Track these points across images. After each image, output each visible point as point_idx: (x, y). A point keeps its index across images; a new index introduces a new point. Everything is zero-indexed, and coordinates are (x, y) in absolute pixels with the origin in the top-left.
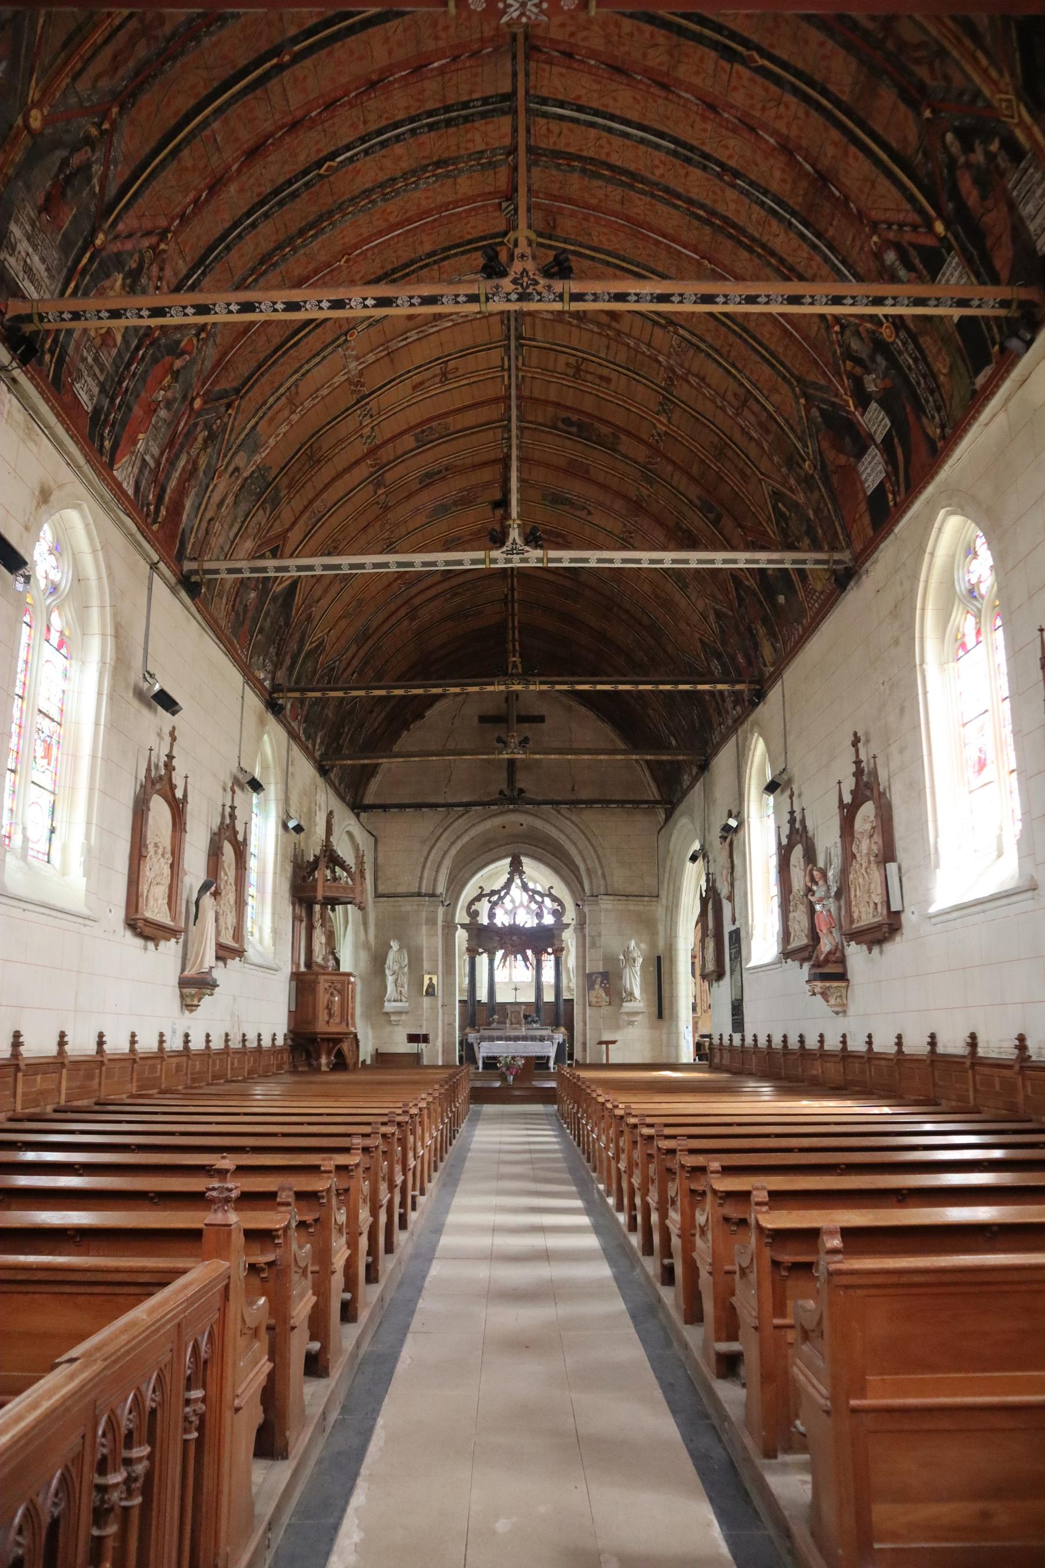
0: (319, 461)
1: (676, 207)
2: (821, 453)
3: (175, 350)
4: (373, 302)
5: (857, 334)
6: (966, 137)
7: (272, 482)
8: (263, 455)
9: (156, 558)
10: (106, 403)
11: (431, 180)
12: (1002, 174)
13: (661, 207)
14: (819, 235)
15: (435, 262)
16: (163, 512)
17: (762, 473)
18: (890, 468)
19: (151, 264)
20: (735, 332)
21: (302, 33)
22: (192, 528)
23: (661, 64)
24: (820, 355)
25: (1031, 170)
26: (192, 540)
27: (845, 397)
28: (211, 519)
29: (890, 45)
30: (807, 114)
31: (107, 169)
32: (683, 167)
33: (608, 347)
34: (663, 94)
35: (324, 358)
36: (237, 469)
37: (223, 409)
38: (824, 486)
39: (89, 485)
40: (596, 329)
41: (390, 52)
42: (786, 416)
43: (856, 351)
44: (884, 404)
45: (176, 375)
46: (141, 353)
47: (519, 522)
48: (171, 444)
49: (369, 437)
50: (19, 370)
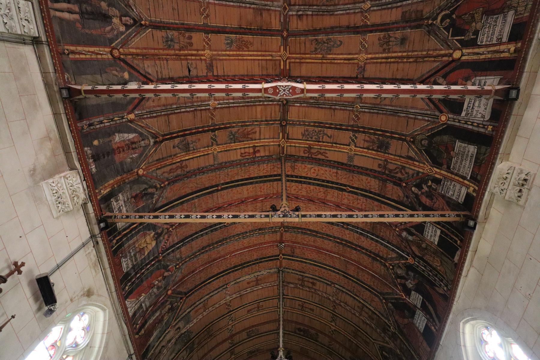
0: (211, 336)
1: (330, 240)
2: (396, 321)
3: (166, 268)
4: (232, 216)
5: (399, 267)
6: (419, 186)
7: (191, 339)
8: (191, 326)
9: (132, 352)
10: (133, 274)
11: (257, 234)
12: (435, 190)
13: (326, 241)
14: (377, 237)
15: (257, 263)
16: (143, 332)
17: (373, 339)
18: (428, 316)
19: (166, 234)
20: (355, 282)
21: (225, 183)
22: (154, 346)
23: (322, 196)
24: (387, 281)
25: (446, 183)
26: (152, 352)
27: (400, 294)
28: (163, 346)
29: (387, 172)
30: (366, 200)
31: (159, 198)
32: (331, 226)
33: (312, 296)
34: (323, 205)
35: (218, 292)
36: (179, 328)
37: (179, 299)
38: (401, 336)
39: (113, 304)
40: (308, 290)
41: (248, 193)
42: (379, 310)
43: (401, 274)
44: (417, 290)
45: (164, 278)
46: (153, 263)
47: (283, 349)
48: (155, 304)
49: (231, 329)
50: (100, 239)
